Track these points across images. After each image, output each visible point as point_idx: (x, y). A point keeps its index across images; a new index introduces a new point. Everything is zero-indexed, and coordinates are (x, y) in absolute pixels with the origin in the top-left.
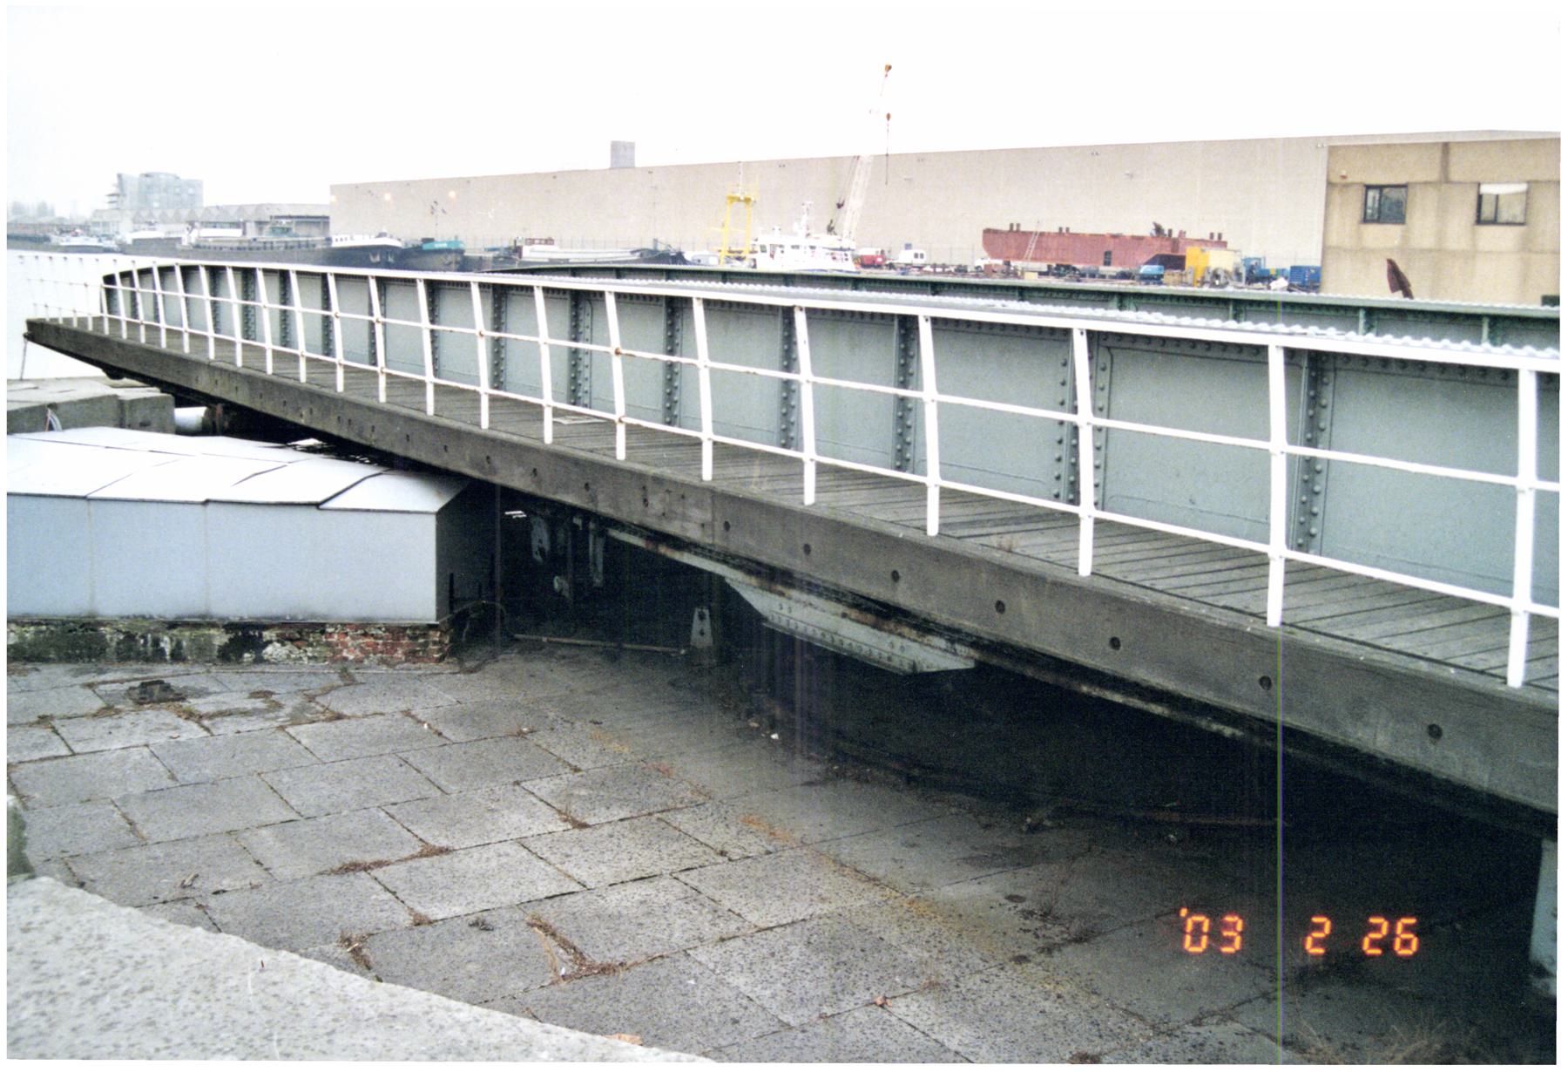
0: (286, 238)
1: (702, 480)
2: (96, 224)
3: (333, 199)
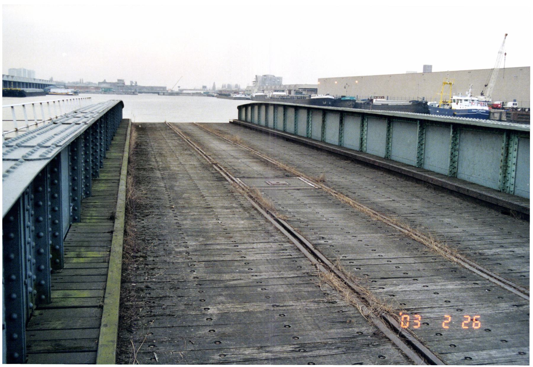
2: (247, 91)
3: (319, 83)
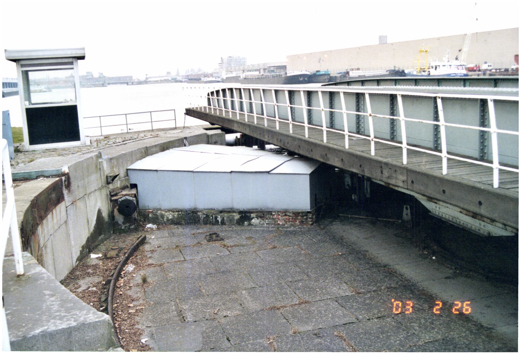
0: (273, 74)
1: (403, 164)
2: (215, 73)
